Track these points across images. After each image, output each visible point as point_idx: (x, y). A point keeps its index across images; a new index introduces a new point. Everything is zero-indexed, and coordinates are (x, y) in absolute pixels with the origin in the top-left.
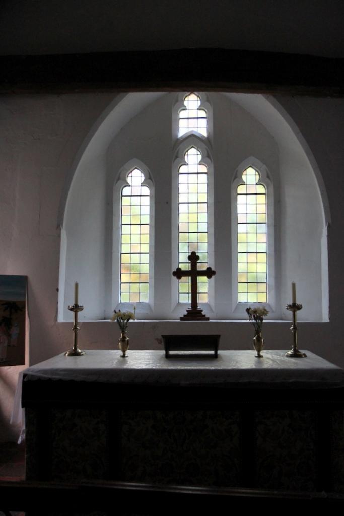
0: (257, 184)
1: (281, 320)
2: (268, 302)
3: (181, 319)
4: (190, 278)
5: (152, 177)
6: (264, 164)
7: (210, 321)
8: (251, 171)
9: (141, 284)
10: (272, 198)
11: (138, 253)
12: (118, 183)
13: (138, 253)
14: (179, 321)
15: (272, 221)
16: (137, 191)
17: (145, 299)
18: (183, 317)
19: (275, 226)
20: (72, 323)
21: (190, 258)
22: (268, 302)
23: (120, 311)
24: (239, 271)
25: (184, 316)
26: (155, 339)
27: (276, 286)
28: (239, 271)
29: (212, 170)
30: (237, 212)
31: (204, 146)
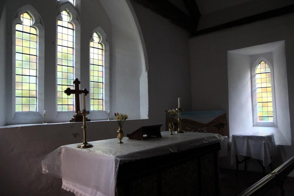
0: (31, 26)
1: (63, 122)
2: (37, 111)
3: (71, 121)
4: (74, 95)
5: (108, 40)
6: (105, 32)
7: (91, 121)
8: (26, 15)
9: (30, 98)
10: (108, 53)
11: (28, 76)
12: (16, 19)
13: (28, 76)
14: (69, 122)
15: (108, 65)
16: (27, 29)
17: (33, 109)
18: (71, 120)
19: (110, 68)
20: (140, 118)
21: (74, 82)
22: (104, 110)
23: (118, 113)
24: (58, 91)
25: (72, 119)
26: (162, 125)
27: (110, 101)
28: (58, 91)
29: (79, 28)
30: (15, 44)
31: (75, 12)
